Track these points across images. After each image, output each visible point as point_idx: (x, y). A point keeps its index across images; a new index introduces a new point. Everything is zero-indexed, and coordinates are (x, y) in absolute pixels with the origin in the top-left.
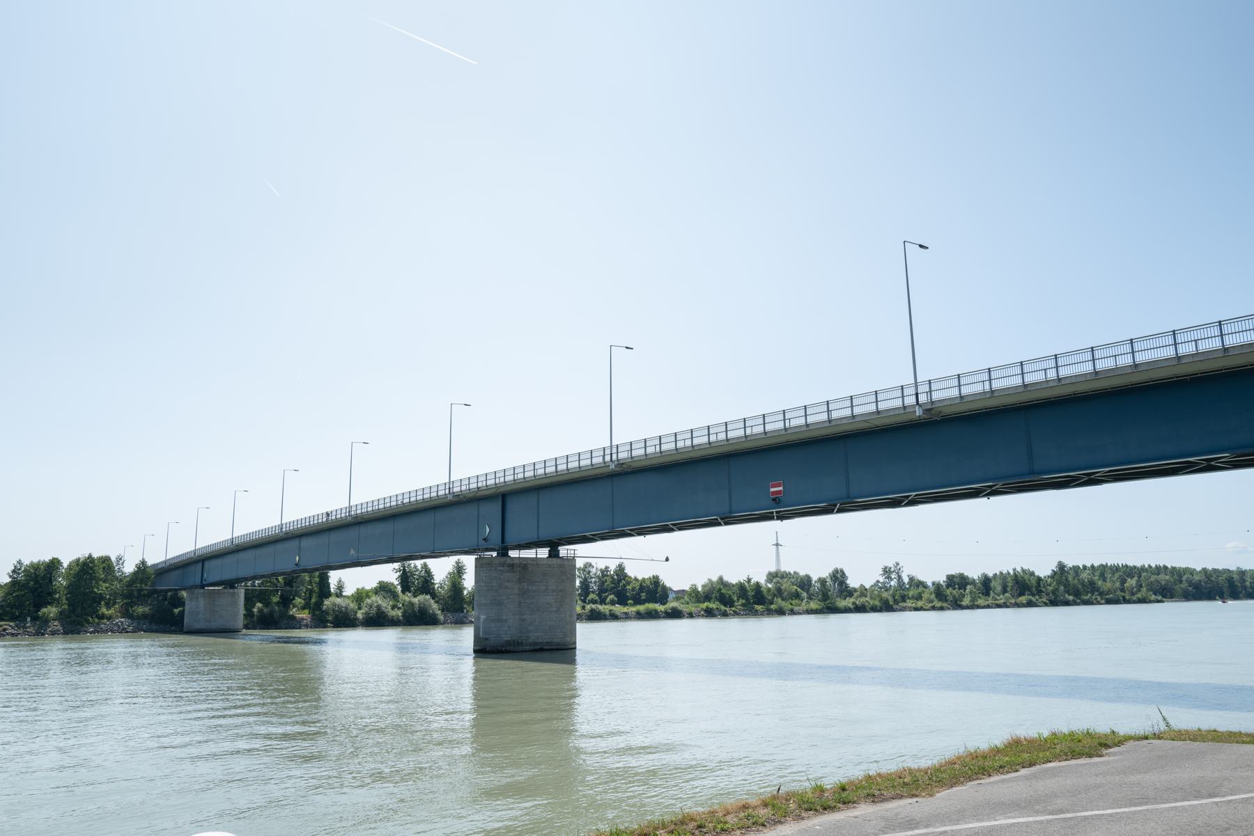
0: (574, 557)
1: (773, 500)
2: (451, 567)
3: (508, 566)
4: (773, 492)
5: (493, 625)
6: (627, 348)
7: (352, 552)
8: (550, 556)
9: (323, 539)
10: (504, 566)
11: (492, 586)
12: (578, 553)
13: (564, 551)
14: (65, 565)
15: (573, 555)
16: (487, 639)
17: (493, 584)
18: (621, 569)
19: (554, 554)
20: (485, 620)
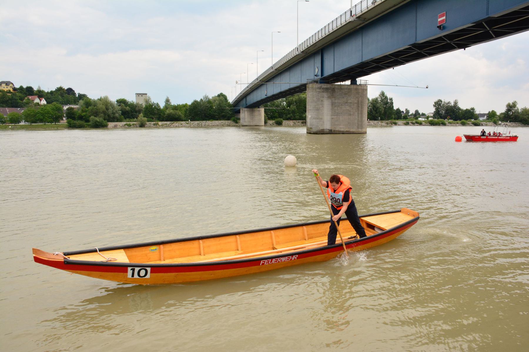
0: (366, 85)
1: (438, 27)
2: (447, 101)
3: (323, 89)
4: (444, 16)
5: (314, 120)
6: (306, 1)
7: (30, 98)
8: (352, 83)
9: (335, 62)
10: (320, 89)
11: (314, 100)
12: (368, 82)
13: (360, 80)
14: (468, 344)
15: (365, 84)
16: (311, 128)
17: (314, 99)
18: (456, 103)
19: (354, 82)
20: (311, 118)
